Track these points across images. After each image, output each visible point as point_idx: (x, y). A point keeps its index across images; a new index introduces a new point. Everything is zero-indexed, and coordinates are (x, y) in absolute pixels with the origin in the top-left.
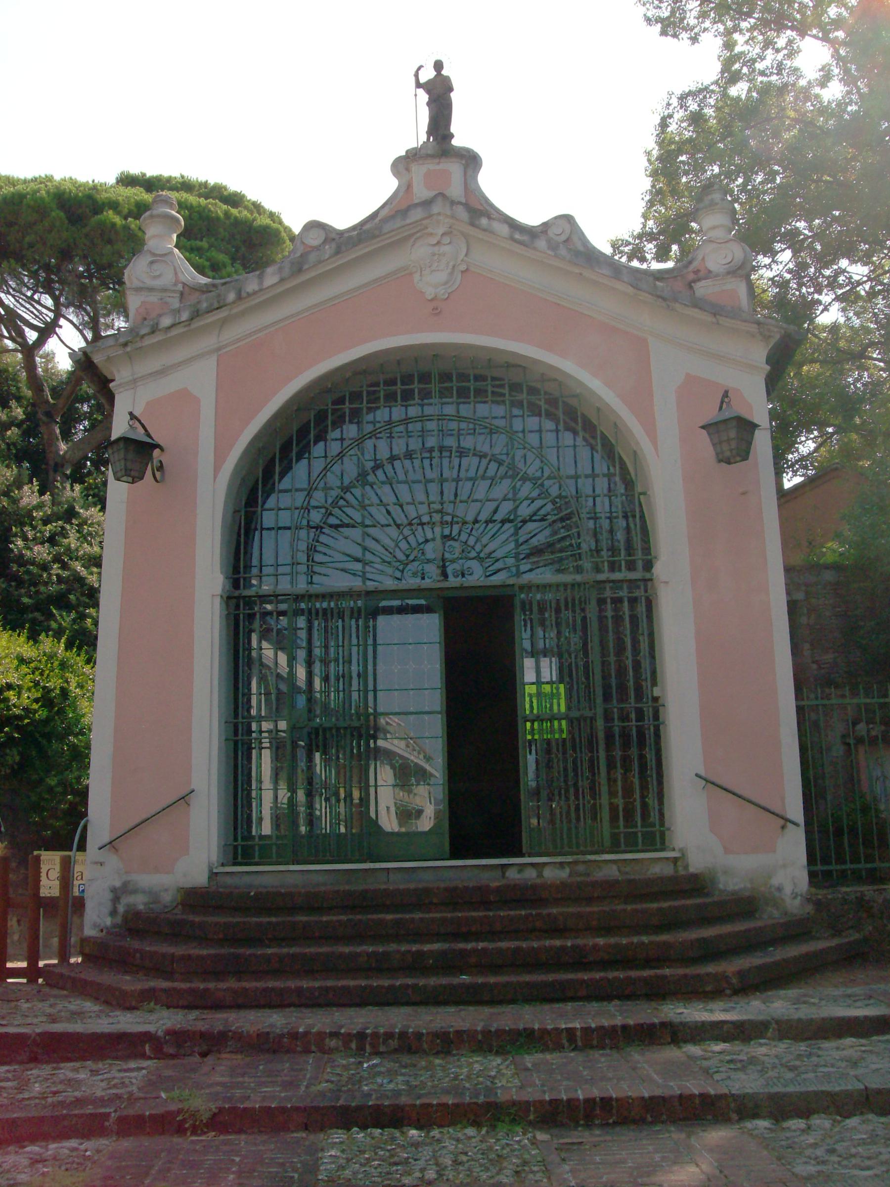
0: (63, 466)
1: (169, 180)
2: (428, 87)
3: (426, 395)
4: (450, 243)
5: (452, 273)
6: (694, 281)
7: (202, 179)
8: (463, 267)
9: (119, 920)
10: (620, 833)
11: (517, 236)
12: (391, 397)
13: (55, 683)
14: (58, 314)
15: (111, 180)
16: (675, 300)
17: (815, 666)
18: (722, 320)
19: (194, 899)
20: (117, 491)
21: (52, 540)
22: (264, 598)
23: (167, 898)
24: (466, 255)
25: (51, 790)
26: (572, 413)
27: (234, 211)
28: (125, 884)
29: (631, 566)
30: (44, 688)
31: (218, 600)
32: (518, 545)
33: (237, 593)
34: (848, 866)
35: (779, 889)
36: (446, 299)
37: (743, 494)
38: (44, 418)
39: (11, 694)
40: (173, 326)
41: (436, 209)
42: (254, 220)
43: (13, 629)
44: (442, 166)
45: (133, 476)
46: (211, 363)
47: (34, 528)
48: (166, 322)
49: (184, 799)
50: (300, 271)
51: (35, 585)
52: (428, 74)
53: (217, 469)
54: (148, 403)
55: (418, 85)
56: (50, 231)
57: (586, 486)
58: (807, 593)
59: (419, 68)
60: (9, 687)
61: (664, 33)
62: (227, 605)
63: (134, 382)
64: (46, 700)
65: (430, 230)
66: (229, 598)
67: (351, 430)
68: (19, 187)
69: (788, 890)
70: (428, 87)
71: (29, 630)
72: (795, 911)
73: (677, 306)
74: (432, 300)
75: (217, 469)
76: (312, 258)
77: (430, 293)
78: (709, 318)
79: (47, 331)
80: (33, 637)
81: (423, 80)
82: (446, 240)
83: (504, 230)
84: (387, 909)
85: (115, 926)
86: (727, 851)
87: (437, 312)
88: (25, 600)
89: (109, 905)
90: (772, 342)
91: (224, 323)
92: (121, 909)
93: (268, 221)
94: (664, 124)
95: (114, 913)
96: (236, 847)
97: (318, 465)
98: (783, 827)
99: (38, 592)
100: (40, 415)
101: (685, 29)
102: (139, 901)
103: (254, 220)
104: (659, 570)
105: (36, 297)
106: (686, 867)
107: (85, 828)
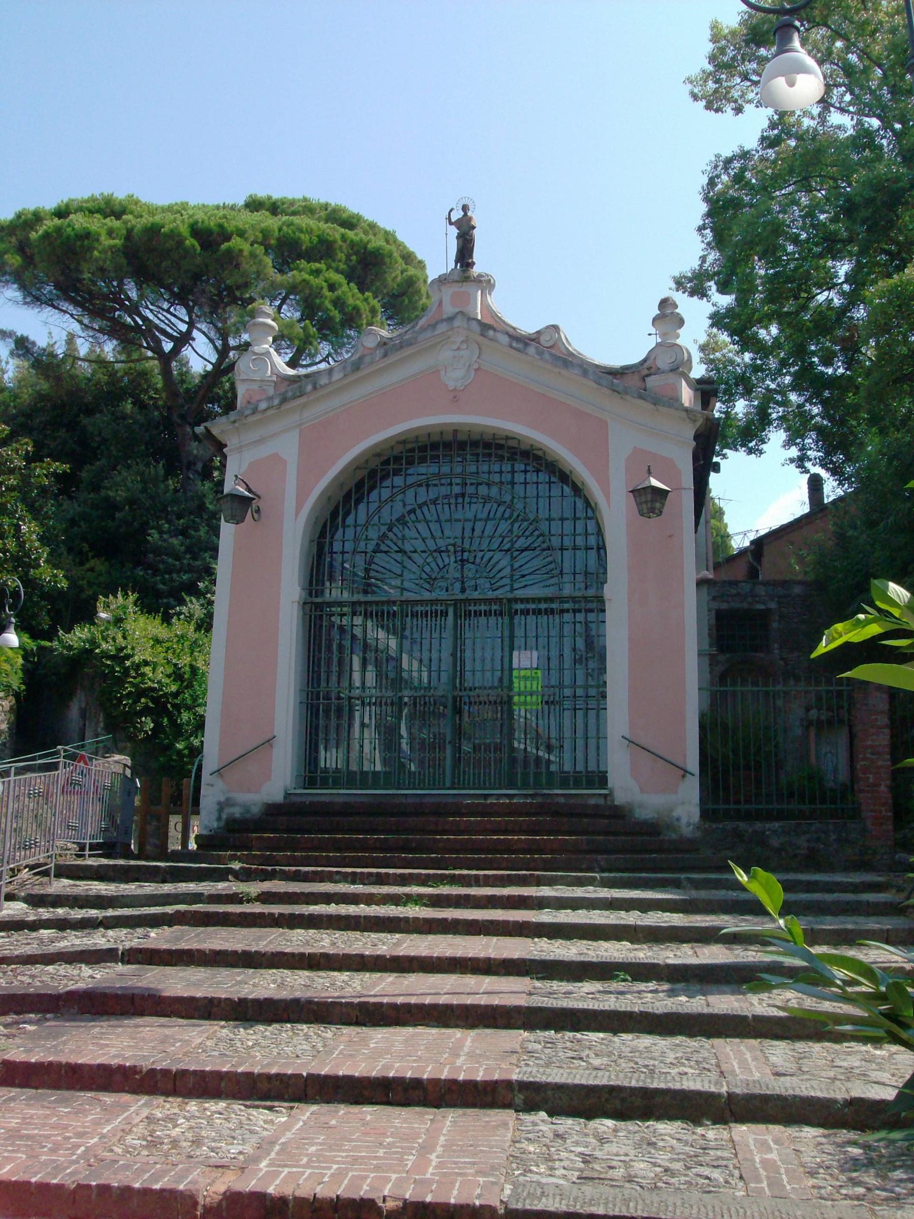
0: (195, 464)
1: (292, 203)
2: (458, 224)
5: (468, 370)
6: (648, 376)
7: (323, 201)
8: (476, 366)
9: (222, 824)
11: (514, 345)
12: (423, 460)
13: (185, 661)
14: (191, 325)
15: (241, 202)
16: (627, 393)
17: (782, 663)
18: (660, 408)
19: (273, 810)
20: (227, 529)
21: (184, 532)
22: (330, 604)
23: (255, 810)
25: (179, 752)
27: (350, 234)
28: (228, 799)
30: (175, 665)
31: (296, 605)
32: (513, 570)
33: (310, 600)
34: (732, 806)
35: (678, 819)
37: (670, 536)
38: (179, 421)
39: (147, 670)
40: (268, 408)
41: (457, 323)
42: (368, 242)
43: (149, 613)
44: (462, 289)
45: (237, 519)
46: (295, 434)
47: (169, 522)
48: (263, 406)
49: (269, 742)
50: (358, 369)
51: (170, 573)
52: (457, 215)
53: (297, 512)
54: (250, 464)
56: (185, 257)
57: (556, 527)
58: (779, 603)
60: (146, 663)
61: (708, 107)
62: (303, 608)
63: (240, 449)
64: (177, 675)
66: (305, 603)
67: (398, 481)
68: (158, 218)
69: (684, 820)
70: (458, 224)
71: (163, 614)
72: (689, 836)
73: (628, 397)
75: (297, 512)
76: (367, 359)
77: (451, 385)
78: (652, 407)
79: (184, 339)
80: (167, 619)
81: (453, 220)
83: (505, 339)
84: (392, 815)
85: (219, 828)
86: (642, 791)
88: (161, 586)
89: (216, 814)
90: (698, 424)
91: (304, 406)
92: (224, 816)
93: (382, 243)
94: (712, 183)
95: (219, 819)
97: (373, 507)
98: (683, 776)
99: (172, 580)
100: (175, 418)
101: (729, 101)
102: (237, 812)
103: (368, 242)
105: (172, 310)
106: (613, 801)
107: (201, 761)
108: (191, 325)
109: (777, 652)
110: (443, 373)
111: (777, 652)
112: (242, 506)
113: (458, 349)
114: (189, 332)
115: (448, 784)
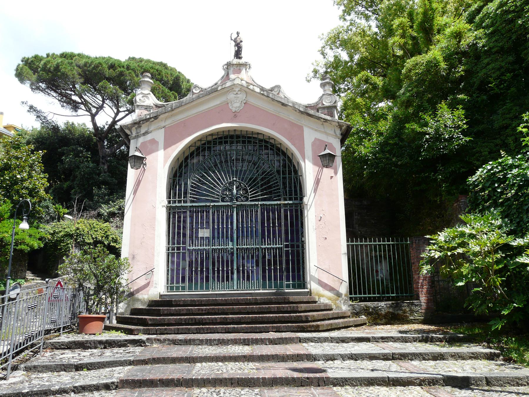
3: (232, 143)
5: (241, 103)
12: (220, 143)
14: (103, 102)
17: (359, 232)
26: (278, 149)
29: (296, 199)
52: (234, 36)
55: (232, 40)
63: (137, 137)
70: (235, 41)
77: (234, 110)
87: (235, 116)
96: (168, 287)
104: (305, 200)
108: (103, 102)
109: (357, 228)
110: (230, 104)
111: (357, 228)
112: (139, 161)
113: (237, 94)
114: (103, 105)
115: (235, 288)
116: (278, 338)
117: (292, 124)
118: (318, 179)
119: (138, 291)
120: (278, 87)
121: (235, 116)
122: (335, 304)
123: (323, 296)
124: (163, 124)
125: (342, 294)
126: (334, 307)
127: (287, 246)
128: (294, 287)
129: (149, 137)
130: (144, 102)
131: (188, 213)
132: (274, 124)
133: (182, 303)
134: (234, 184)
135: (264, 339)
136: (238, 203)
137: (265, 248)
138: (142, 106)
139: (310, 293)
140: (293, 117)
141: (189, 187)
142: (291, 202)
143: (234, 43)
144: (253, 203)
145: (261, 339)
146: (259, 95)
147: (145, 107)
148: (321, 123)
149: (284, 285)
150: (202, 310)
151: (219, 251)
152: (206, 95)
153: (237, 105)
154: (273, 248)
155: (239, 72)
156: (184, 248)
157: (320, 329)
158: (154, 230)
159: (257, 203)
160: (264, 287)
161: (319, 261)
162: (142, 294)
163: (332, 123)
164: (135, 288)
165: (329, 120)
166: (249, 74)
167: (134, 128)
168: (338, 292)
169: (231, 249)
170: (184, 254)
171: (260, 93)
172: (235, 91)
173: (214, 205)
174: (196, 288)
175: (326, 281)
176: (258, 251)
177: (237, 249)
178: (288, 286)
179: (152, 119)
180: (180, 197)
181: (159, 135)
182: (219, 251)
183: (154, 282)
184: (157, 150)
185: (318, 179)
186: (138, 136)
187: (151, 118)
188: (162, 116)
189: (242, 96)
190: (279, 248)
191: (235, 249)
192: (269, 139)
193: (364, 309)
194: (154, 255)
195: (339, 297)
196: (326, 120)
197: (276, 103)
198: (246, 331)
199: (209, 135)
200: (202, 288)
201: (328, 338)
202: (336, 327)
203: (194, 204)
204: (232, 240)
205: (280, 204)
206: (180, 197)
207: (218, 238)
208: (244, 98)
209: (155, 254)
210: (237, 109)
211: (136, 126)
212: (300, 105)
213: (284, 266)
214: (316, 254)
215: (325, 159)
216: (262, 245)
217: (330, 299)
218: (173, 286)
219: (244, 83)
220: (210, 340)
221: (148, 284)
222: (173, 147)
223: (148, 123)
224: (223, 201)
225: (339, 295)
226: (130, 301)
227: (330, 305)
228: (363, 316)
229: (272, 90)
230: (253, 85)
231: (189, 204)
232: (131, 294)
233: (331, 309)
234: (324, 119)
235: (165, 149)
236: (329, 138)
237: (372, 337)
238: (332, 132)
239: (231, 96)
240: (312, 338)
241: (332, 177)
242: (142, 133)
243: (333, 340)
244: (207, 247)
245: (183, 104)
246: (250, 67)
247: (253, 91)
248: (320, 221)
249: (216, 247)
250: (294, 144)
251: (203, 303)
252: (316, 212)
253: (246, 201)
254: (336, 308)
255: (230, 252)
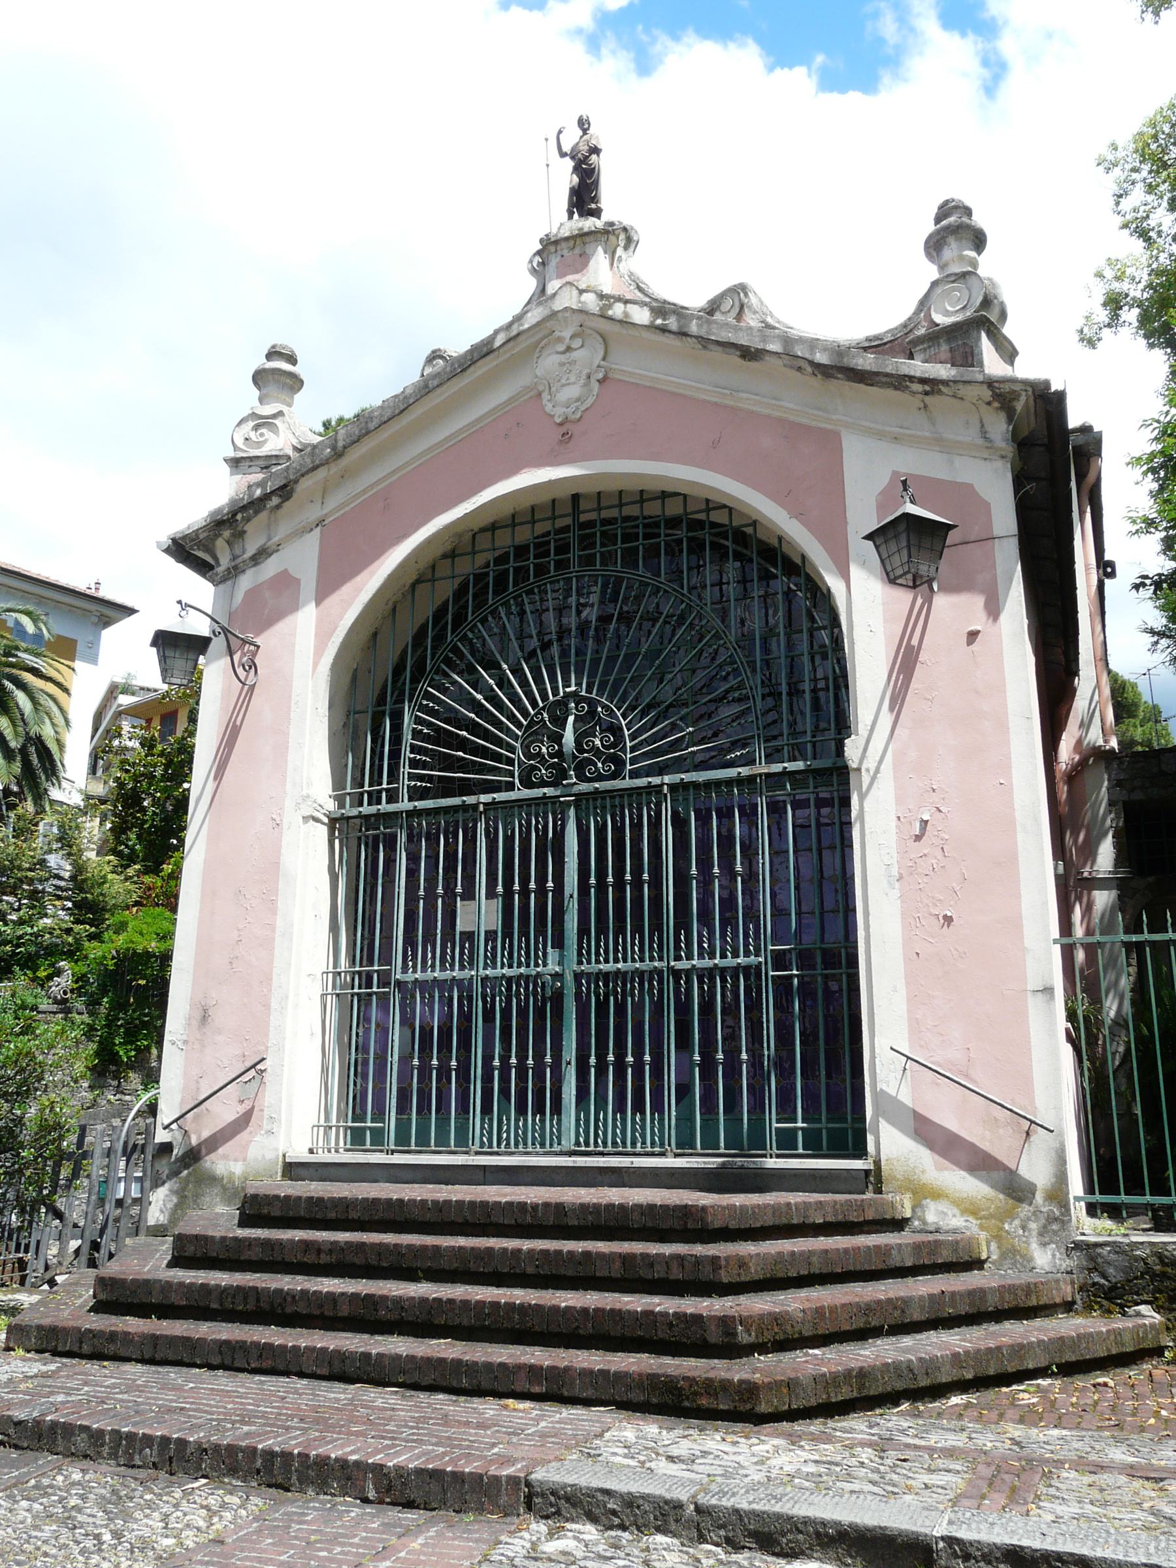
4: (582, 346)
5: (587, 384)
10: (796, 1129)
24: (604, 359)
36: (579, 420)
46: (313, 540)
59: (560, 132)
65: (557, 334)
74: (561, 424)
77: (559, 413)
82: (577, 343)
87: (566, 437)
113: (569, 349)
115: (568, 1142)
116: (419, 1472)
117: (793, 431)
118: (909, 647)
119: (214, 1142)
120: (739, 291)
121: (565, 439)
122: (998, 1238)
123: (937, 1195)
124: (314, 512)
125: (1031, 1189)
126: (988, 1250)
127: (780, 961)
128: (814, 1147)
129: (271, 567)
130: (259, 444)
131: (402, 838)
132: (715, 445)
133: (276, 1213)
134: (567, 713)
135: (357, 1463)
136: (584, 787)
137: (688, 973)
138: (251, 459)
139: (874, 1179)
140: (797, 400)
141: (407, 738)
142: (799, 765)
143: (569, 164)
144: (641, 782)
145: (343, 1463)
146: (646, 334)
147: (262, 463)
148: (916, 401)
149: (771, 1139)
150: (319, 1251)
151: (509, 989)
152: (454, 376)
153: (573, 391)
154: (723, 971)
155: (583, 262)
156: (384, 981)
157: (763, 1408)
158: (274, 911)
159: (656, 780)
160: (685, 1144)
161: (915, 1026)
162: (225, 1157)
163: (963, 390)
164: (206, 1134)
165: (946, 383)
166: (624, 267)
167: (220, 543)
168: (1012, 1174)
169: (557, 976)
170: (384, 999)
171: (651, 327)
172: (560, 340)
173: (494, 803)
174: (423, 1141)
175: (951, 1123)
176: (661, 982)
177: (578, 977)
178: (786, 1142)
179: (275, 500)
180: (376, 779)
181: (301, 557)
182: (509, 989)
183: (266, 1113)
184: (294, 607)
185: (909, 647)
186: (235, 568)
187: (266, 497)
188: (305, 484)
189: (587, 356)
190: (747, 969)
191: (569, 978)
192: (708, 510)
193: (1148, 1270)
194: (267, 1007)
195: (1020, 1200)
196: (932, 385)
197: (717, 354)
198: (415, 1378)
199: (483, 530)
200: (442, 1140)
201: (678, 1506)
202: (900, 1385)
203: (421, 804)
204: (559, 943)
205: (751, 779)
206: (376, 779)
207: (524, 933)
208: (598, 360)
209: (274, 1004)
210: (571, 410)
211: (227, 534)
212: (813, 343)
213: (769, 1048)
214: (903, 992)
215: (893, 546)
216: (678, 958)
217: (970, 1209)
218: (364, 1129)
219: (590, 300)
220: (131, 1436)
221: (243, 1122)
222: (347, 589)
223: (263, 515)
224: (527, 783)
225: (1016, 1190)
226: (187, 1181)
227: (971, 1243)
228: (1143, 1309)
229: (713, 307)
230: (626, 302)
231: (405, 805)
232: (193, 1156)
233: (977, 1264)
234: (923, 381)
235: (318, 604)
236: (958, 461)
237: (950, 1540)
238: (971, 435)
239: (549, 362)
240: (592, 1493)
241: (973, 636)
242: (247, 555)
243: (706, 1523)
244: (467, 973)
245: (372, 426)
246: (629, 240)
247: (625, 323)
248: (918, 838)
249: (499, 972)
250: (798, 514)
251: (354, 1215)
252: (899, 800)
253: (614, 776)
254: (1003, 1256)
255: (549, 993)
